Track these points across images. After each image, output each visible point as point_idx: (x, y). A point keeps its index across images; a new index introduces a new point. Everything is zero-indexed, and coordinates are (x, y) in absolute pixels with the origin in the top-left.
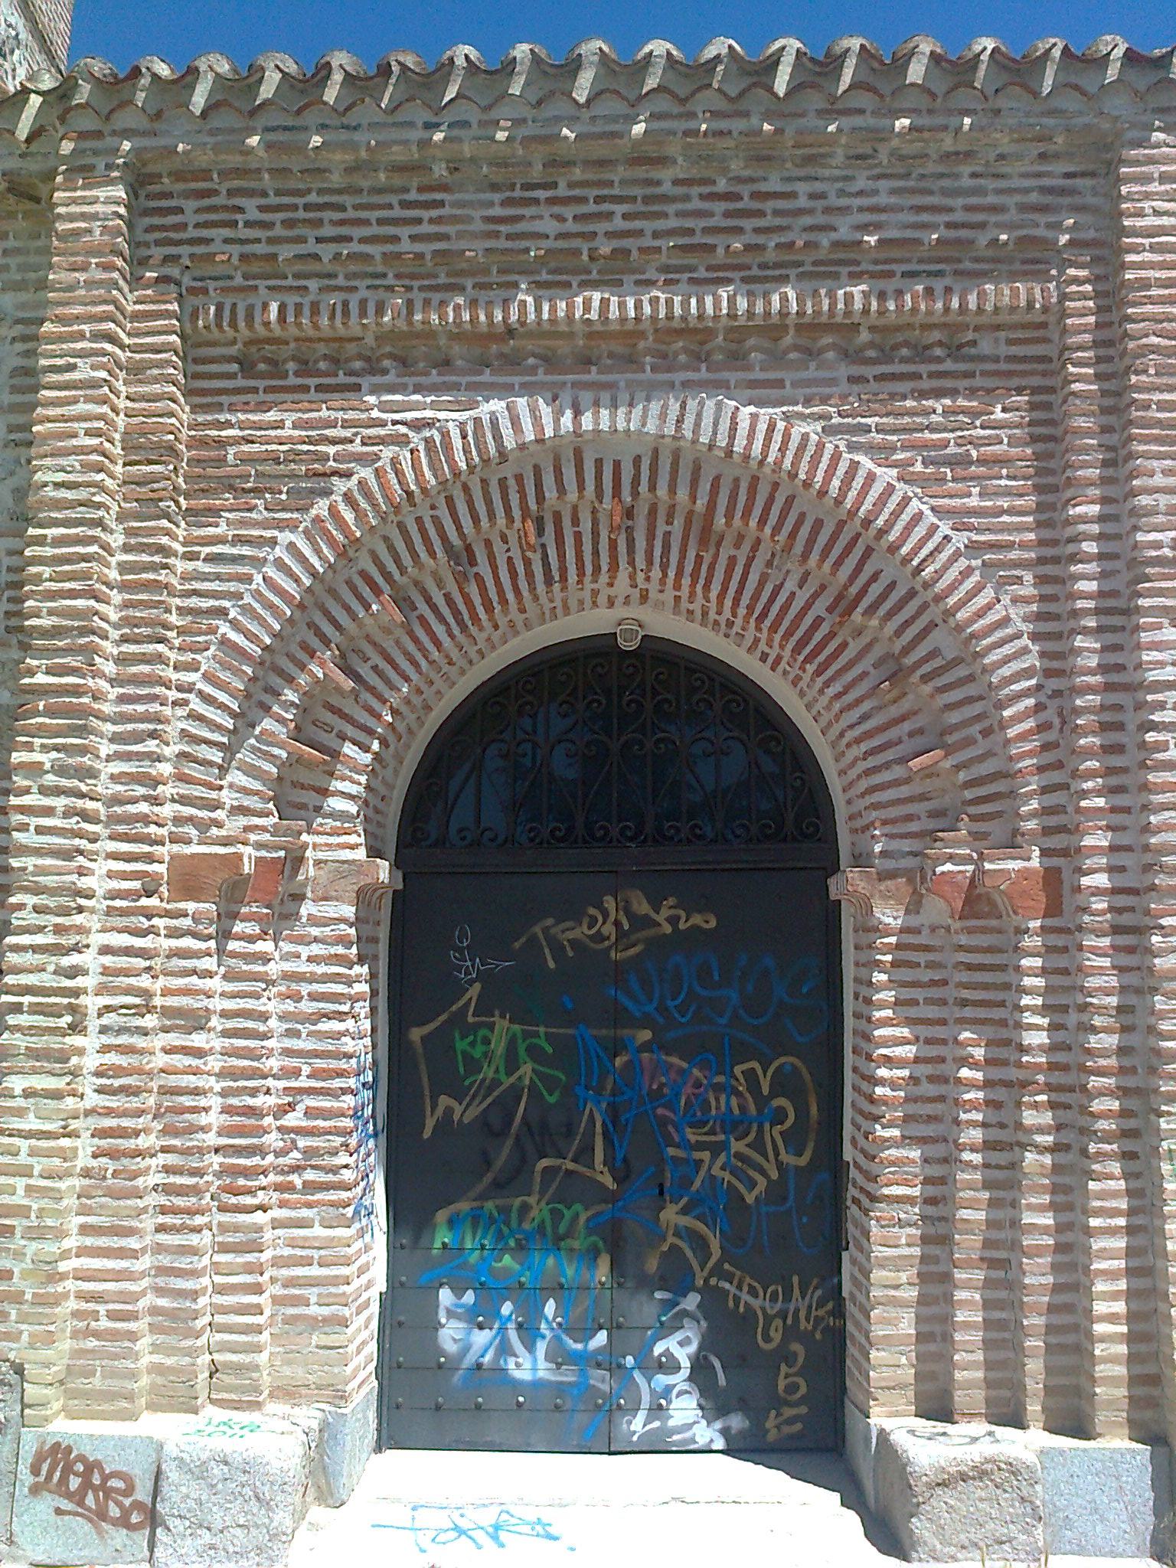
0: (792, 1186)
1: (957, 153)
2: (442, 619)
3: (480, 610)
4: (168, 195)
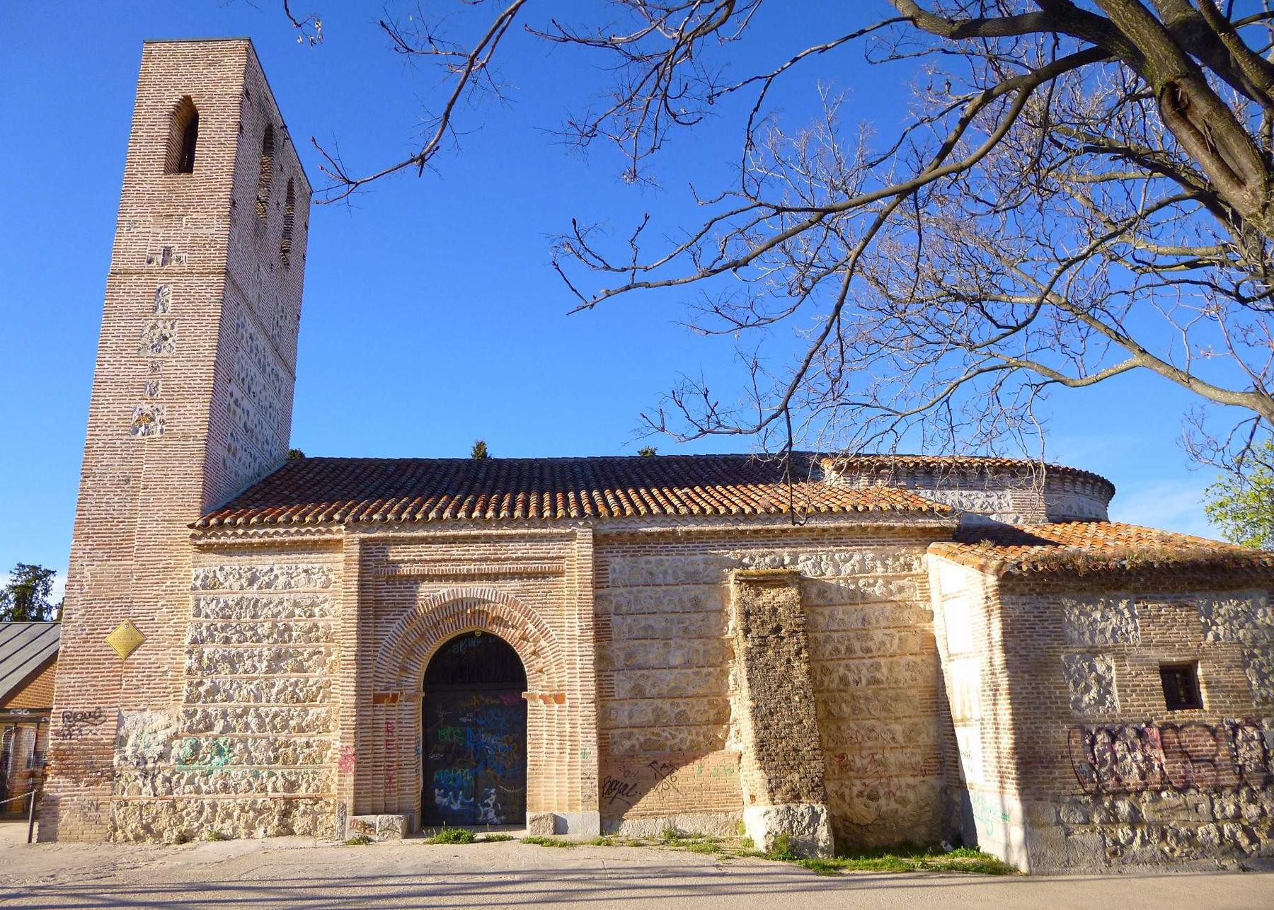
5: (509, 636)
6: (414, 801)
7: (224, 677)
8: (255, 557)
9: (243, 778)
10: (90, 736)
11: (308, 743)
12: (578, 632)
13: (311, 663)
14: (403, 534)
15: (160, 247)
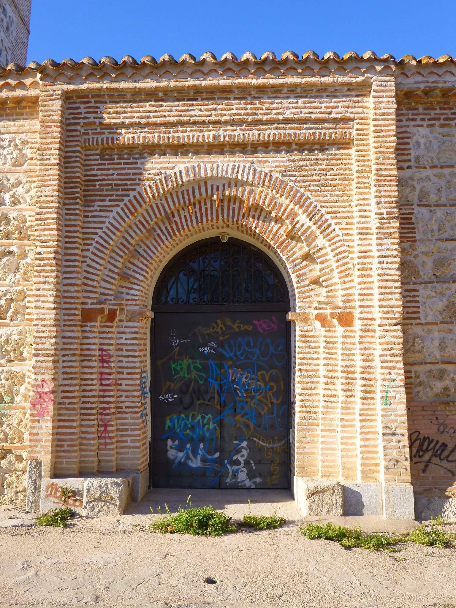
0: (275, 409)
1: (322, 89)
2: (164, 235)
3: (176, 232)
4: (75, 103)
6: (138, 456)
12: (374, 223)
14: (122, 85)
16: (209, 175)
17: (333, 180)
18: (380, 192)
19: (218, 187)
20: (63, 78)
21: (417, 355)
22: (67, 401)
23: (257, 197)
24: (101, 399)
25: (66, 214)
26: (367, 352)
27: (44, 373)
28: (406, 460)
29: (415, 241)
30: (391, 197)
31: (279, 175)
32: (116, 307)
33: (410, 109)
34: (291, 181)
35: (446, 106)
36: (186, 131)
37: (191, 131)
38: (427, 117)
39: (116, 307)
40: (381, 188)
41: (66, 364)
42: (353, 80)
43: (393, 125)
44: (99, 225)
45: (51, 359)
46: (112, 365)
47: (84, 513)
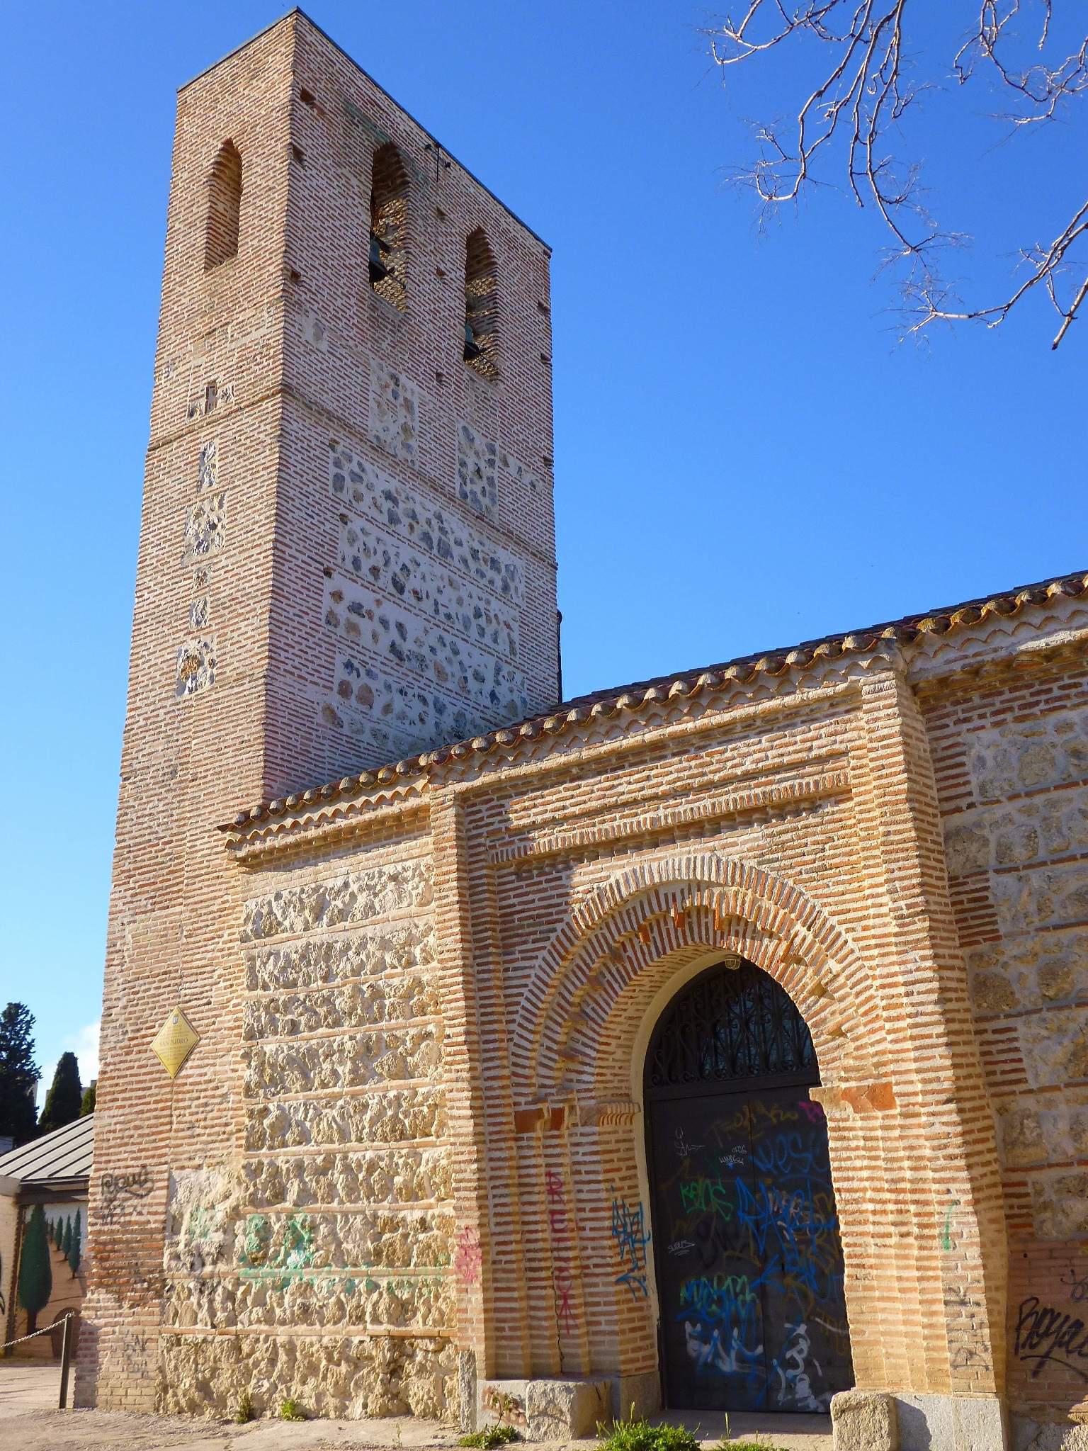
2: (616, 981)
5: (765, 954)
7: (294, 1099)
8: (321, 866)
9: (331, 1293)
10: (134, 1218)
11: (423, 1221)
13: (417, 1058)
15: (203, 385)
16: (657, 880)
17: (833, 857)
18: (893, 871)
19: (674, 895)
20: (454, 775)
21: (1032, 1150)
22: (504, 1258)
23: (731, 903)
24: (556, 1254)
25: (479, 972)
26: (915, 1153)
27: (467, 1217)
28: (986, 1350)
29: (999, 938)
30: (911, 877)
31: (753, 863)
32: (561, 1105)
33: (957, 703)
34: (773, 869)
35: (1019, 684)
36: (614, 819)
37: (621, 818)
38: (988, 710)
39: (561, 1105)
40: (894, 866)
41: (497, 1201)
42: (830, 691)
43: (898, 754)
44: (523, 981)
45: (474, 1194)
46: (565, 1197)
47: (527, 1434)
